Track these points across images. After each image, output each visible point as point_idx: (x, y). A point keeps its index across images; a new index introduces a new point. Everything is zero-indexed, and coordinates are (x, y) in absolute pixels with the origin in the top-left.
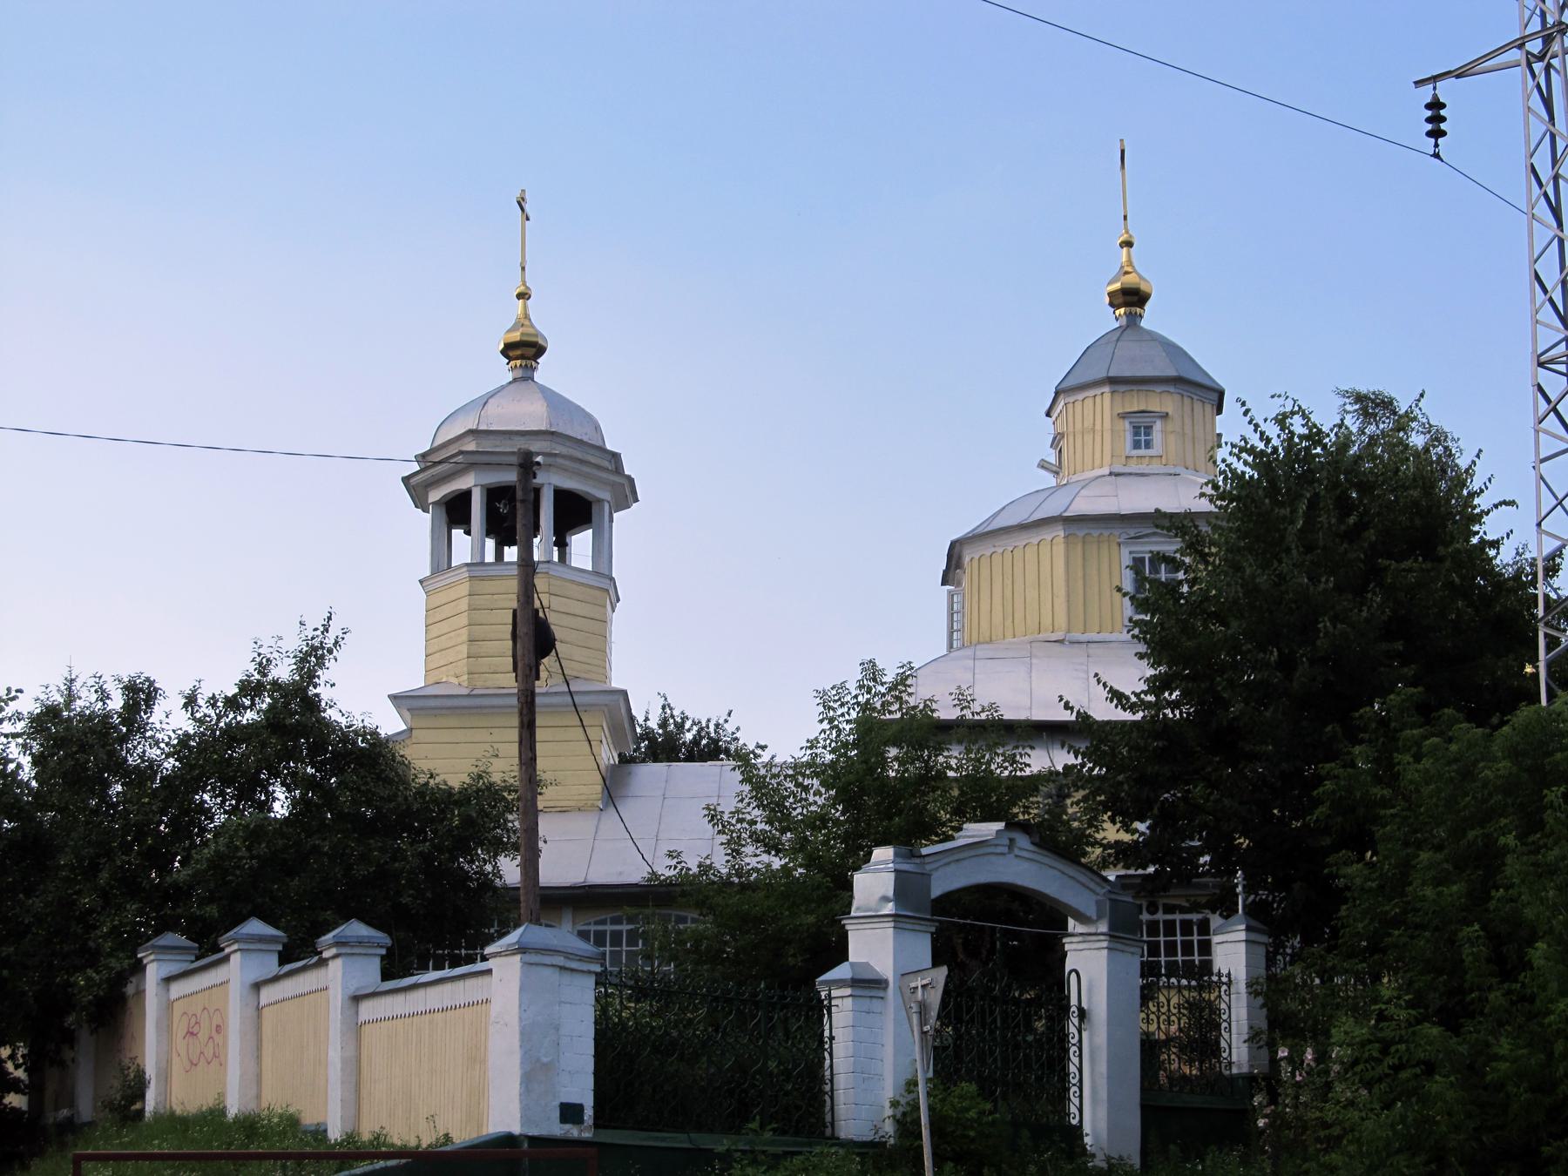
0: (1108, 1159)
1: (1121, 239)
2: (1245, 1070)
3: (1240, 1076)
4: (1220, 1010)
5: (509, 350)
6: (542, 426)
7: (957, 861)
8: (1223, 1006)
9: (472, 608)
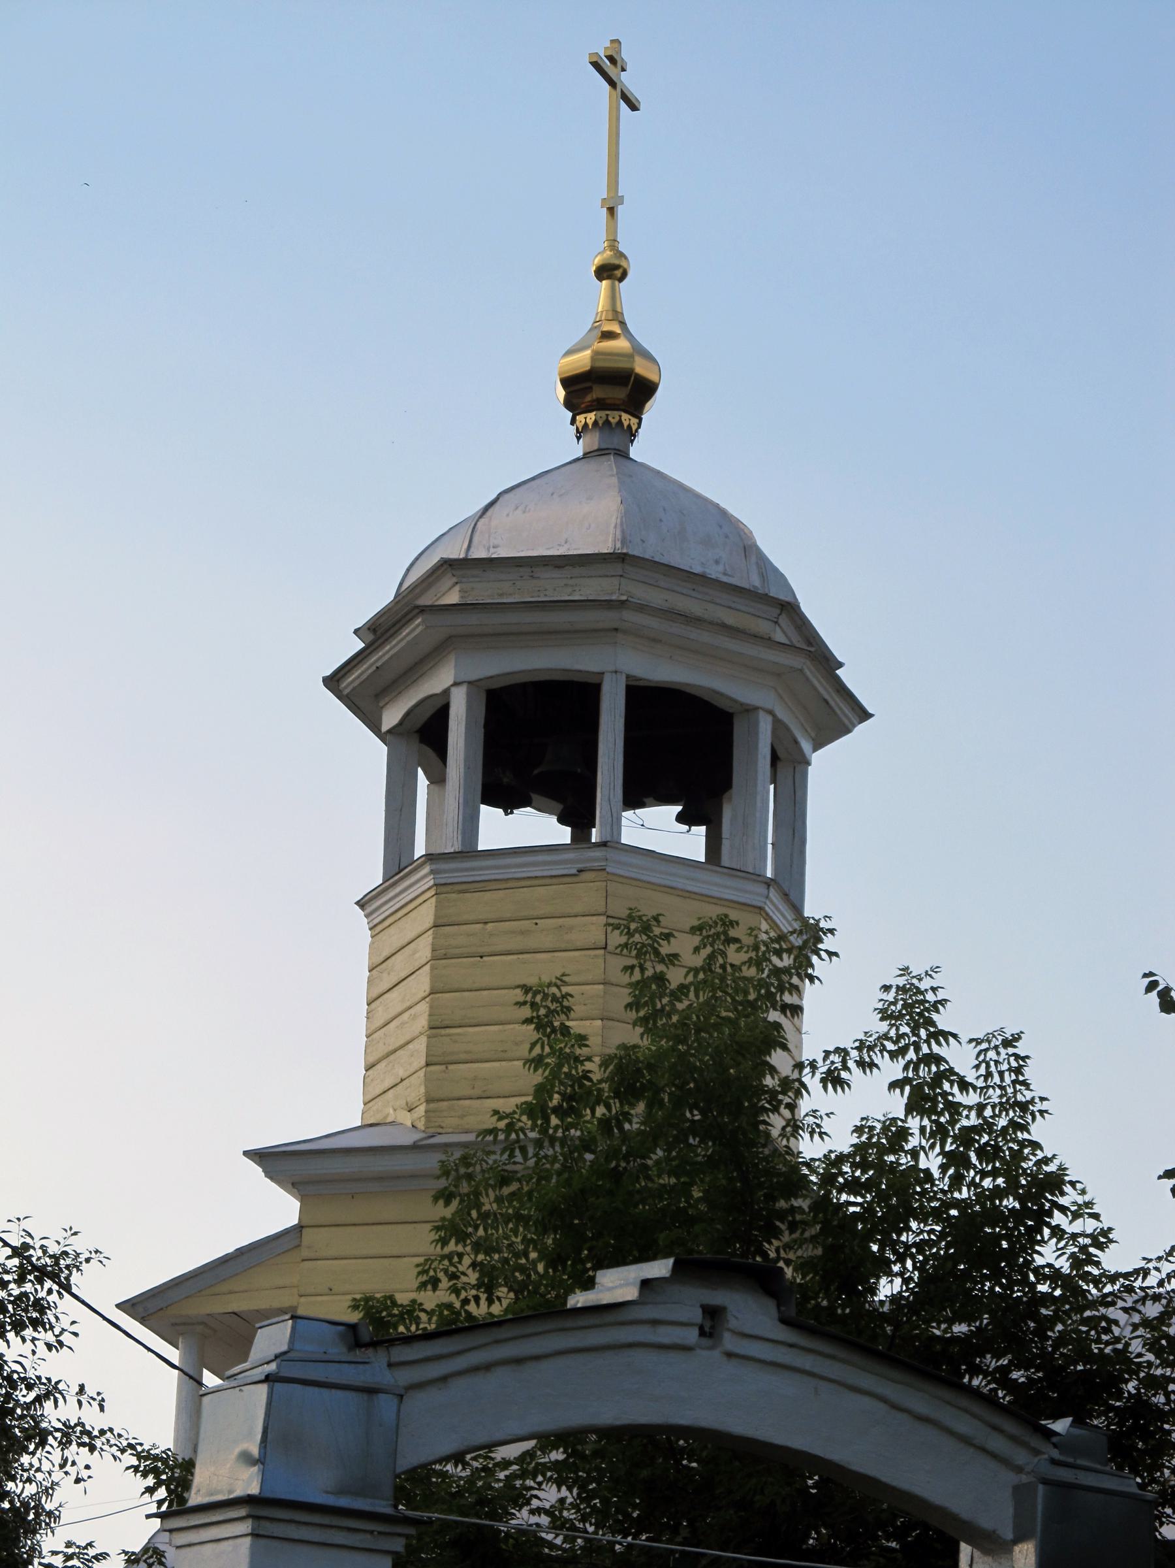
6: (605, 546)
7: (518, 1361)
9: (439, 955)
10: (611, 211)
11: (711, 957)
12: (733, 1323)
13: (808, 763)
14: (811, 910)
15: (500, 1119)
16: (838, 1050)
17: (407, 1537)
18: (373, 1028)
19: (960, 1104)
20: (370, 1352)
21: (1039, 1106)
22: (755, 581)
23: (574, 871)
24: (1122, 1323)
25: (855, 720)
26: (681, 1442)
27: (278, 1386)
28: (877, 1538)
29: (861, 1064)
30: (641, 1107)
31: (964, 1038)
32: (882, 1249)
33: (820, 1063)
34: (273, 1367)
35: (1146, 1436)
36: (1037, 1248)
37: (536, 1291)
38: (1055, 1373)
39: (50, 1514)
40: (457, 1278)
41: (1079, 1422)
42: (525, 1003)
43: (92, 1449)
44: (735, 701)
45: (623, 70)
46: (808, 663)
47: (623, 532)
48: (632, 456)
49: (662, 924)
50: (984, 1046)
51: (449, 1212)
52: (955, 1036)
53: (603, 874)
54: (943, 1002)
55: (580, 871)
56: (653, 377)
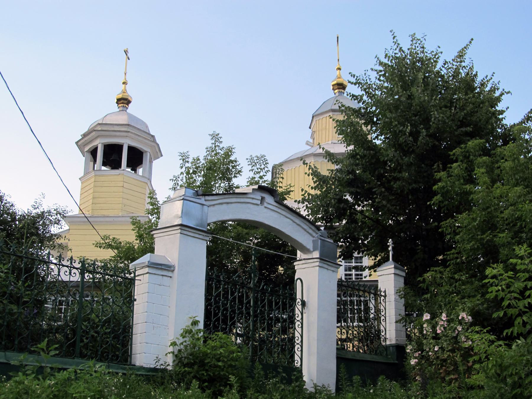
0: (315, 386)
1: (337, 67)
2: (394, 342)
3: (391, 346)
4: (380, 310)
5: (119, 101)
7: (228, 203)
8: (382, 308)
9: (95, 186)
12: (266, 201)
20: (201, 197)
22: (148, 132)
27: (185, 201)
43: (63, 250)
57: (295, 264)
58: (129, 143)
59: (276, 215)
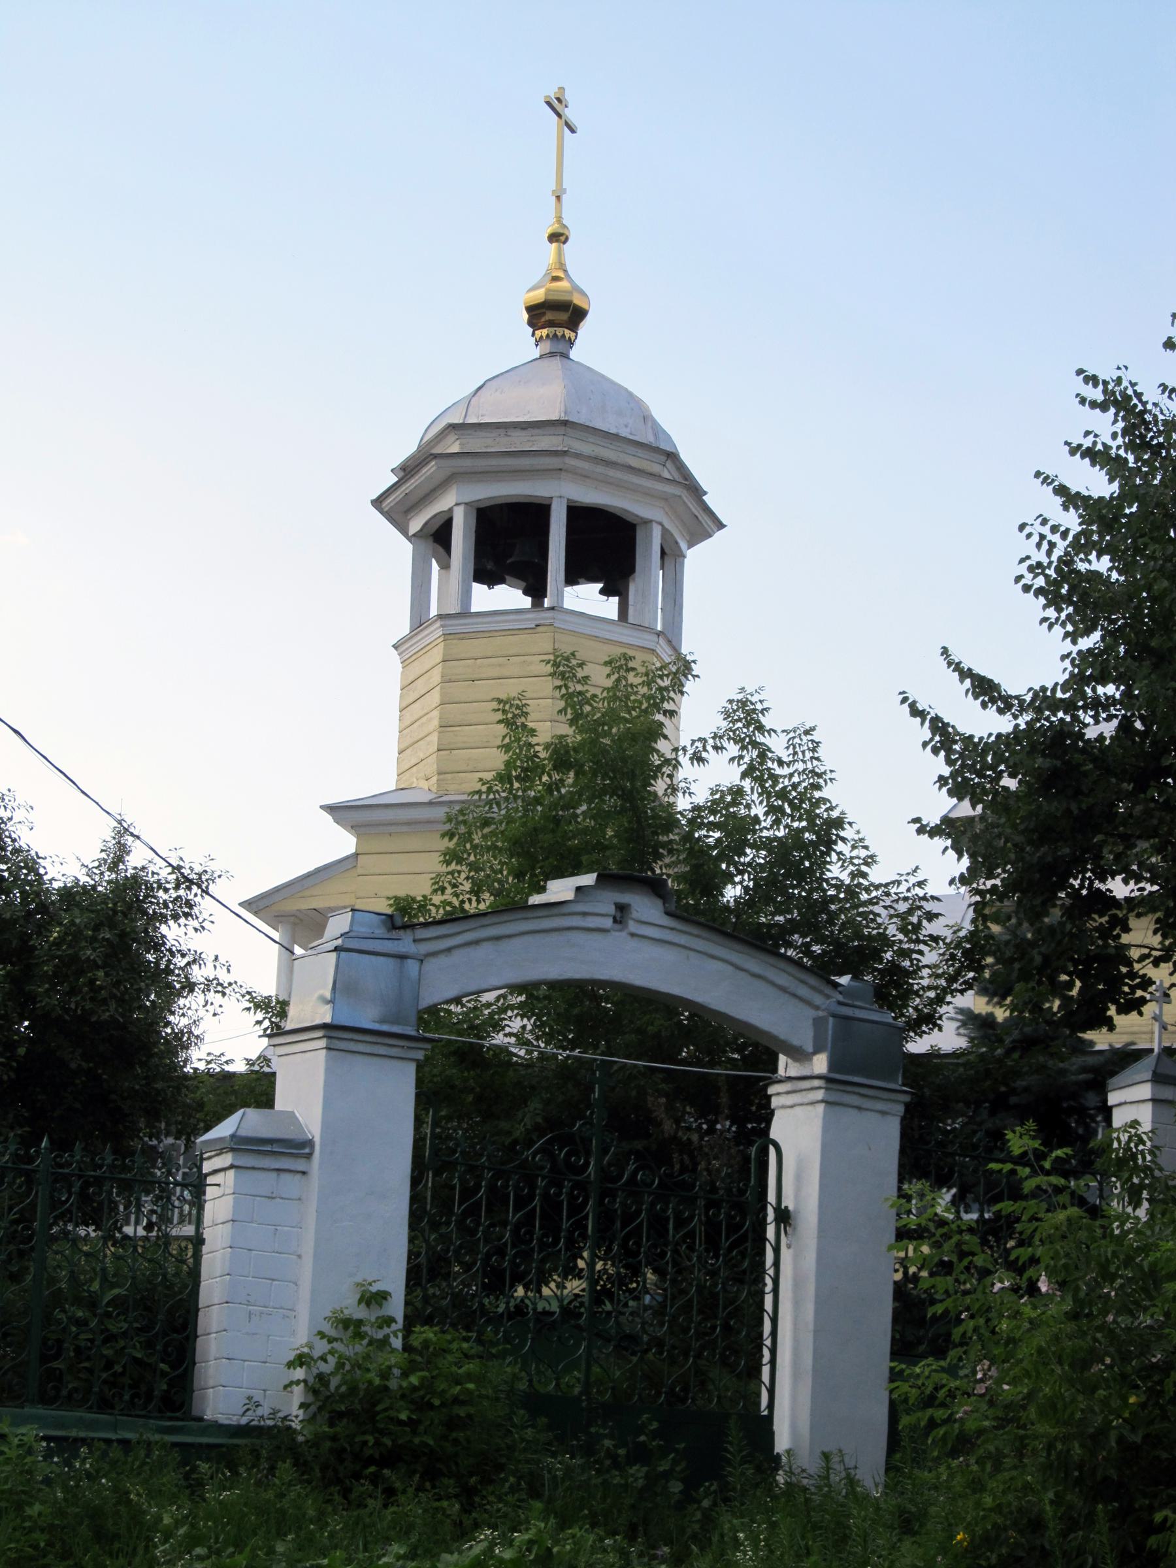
6: (553, 414)
7: (498, 938)
9: (446, 680)
10: (558, 198)
11: (618, 680)
12: (635, 915)
13: (684, 557)
14: (684, 651)
15: (483, 784)
16: (700, 739)
17: (425, 1049)
18: (403, 726)
19: (778, 775)
20: (402, 932)
21: (829, 776)
22: (649, 438)
23: (533, 626)
24: (883, 916)
25: (715, 528)
26: (601, 991)
27: (343, 954)
28: (726, 1052)
29: (716, 748)
30: (572, 774)
31: (779, 731)
32: (728, 867)
33: (689, 748)
34: (339, 942)
35: (898, 986)
36: (828, 866)
37: (508, 896)
38: (839, 946)
39: (197, 1037)
40: (457, 887)
41: (855, 977)
42: (498, 710)
43: (224, 994)
44: (637, 516)
45: (566, 106)
46: (685, 492)
47: (565, 406)
48: (571, 357)
49: (577, 657)
50: (792, 735)
51: (451, 845)
52: (775, 731)
53: (552, 627)
54: (767, 709)
55: (537, 626)
56: (585, 306)
57: (771, 1090)
58: (467, 501)
59: (670, 955)
